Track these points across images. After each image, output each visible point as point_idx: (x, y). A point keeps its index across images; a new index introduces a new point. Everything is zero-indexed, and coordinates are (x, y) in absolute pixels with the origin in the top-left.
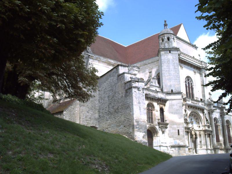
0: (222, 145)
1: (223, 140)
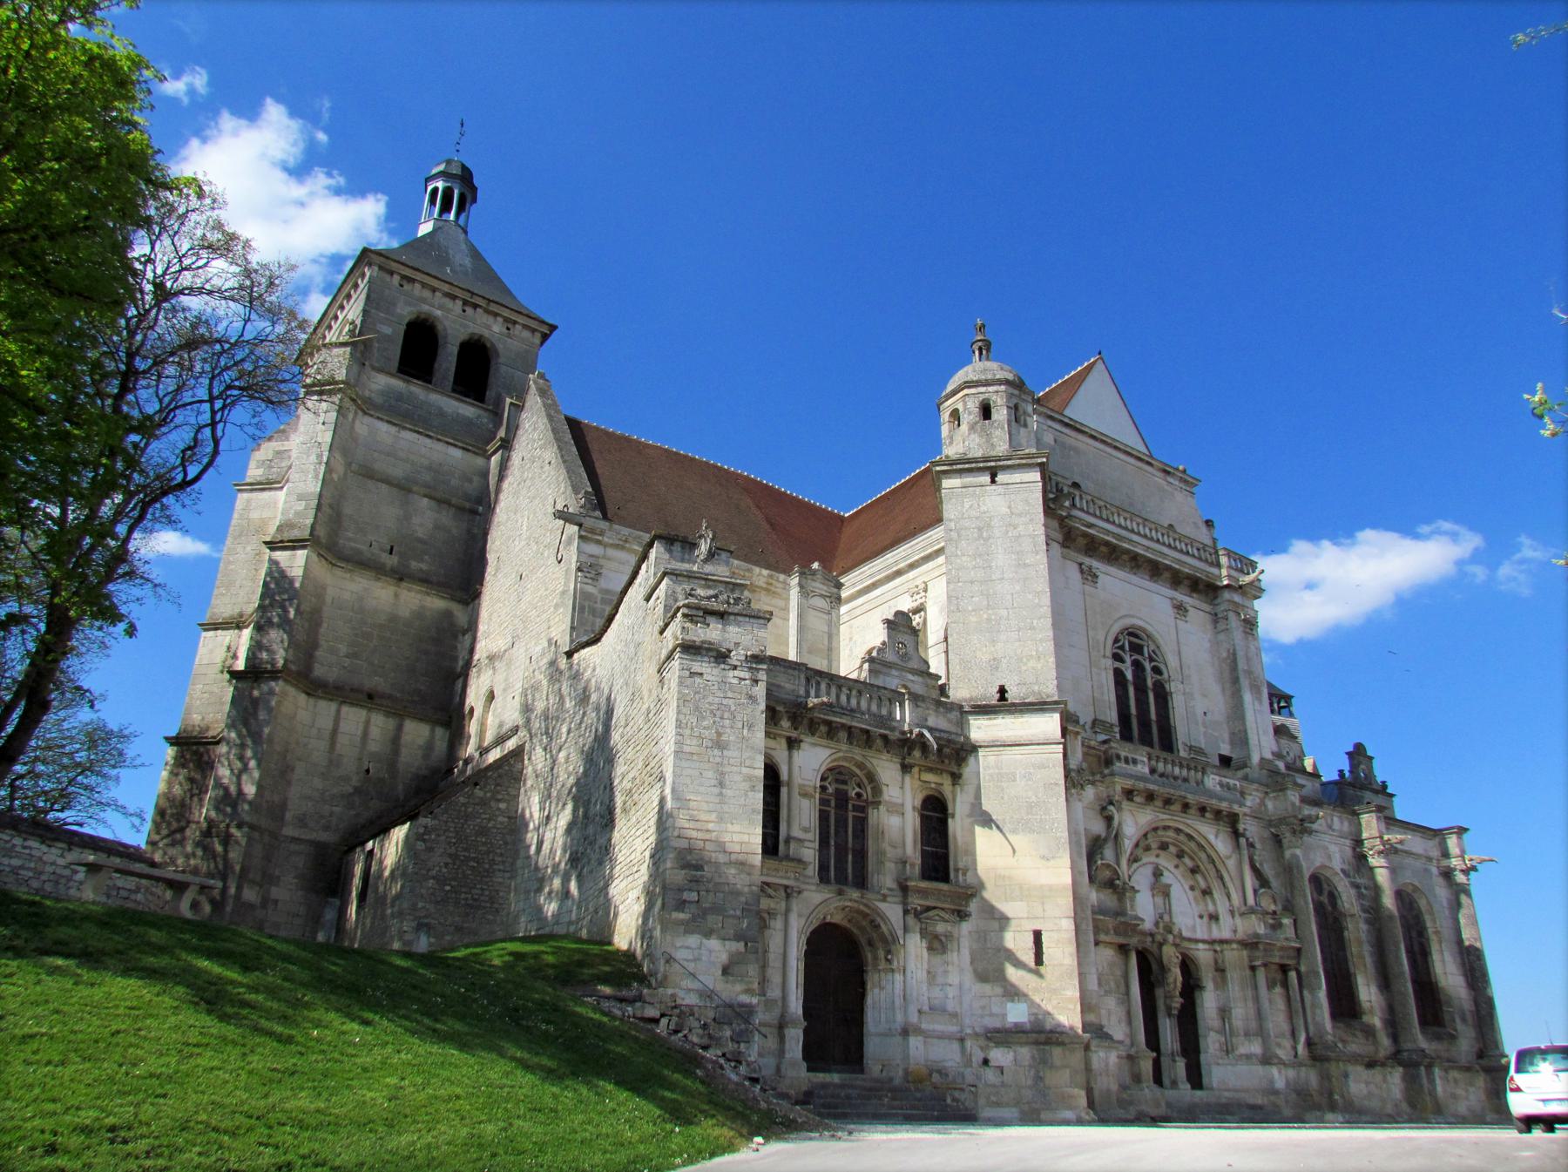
0: (1374, 1036)
1: (1383, 1004)
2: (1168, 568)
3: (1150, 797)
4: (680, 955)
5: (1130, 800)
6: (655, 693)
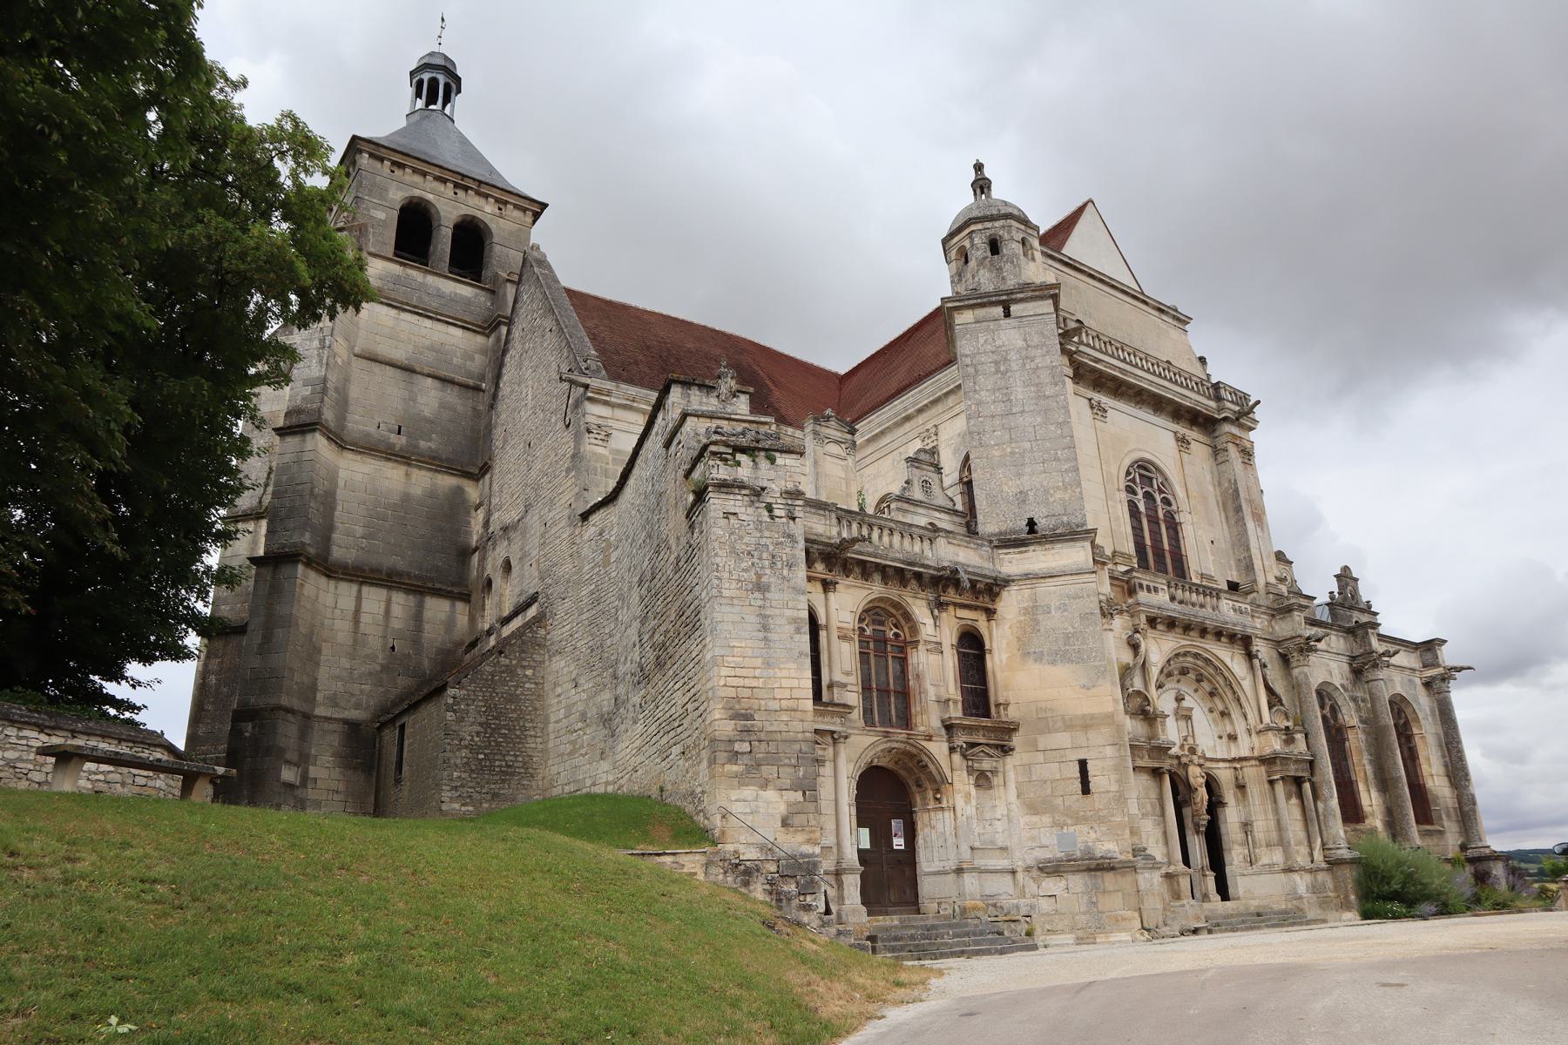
2: (1170, 401)
3: (1171, 624)
4: (736, 808)
5: (1153, 627)
6: (683, 541)
